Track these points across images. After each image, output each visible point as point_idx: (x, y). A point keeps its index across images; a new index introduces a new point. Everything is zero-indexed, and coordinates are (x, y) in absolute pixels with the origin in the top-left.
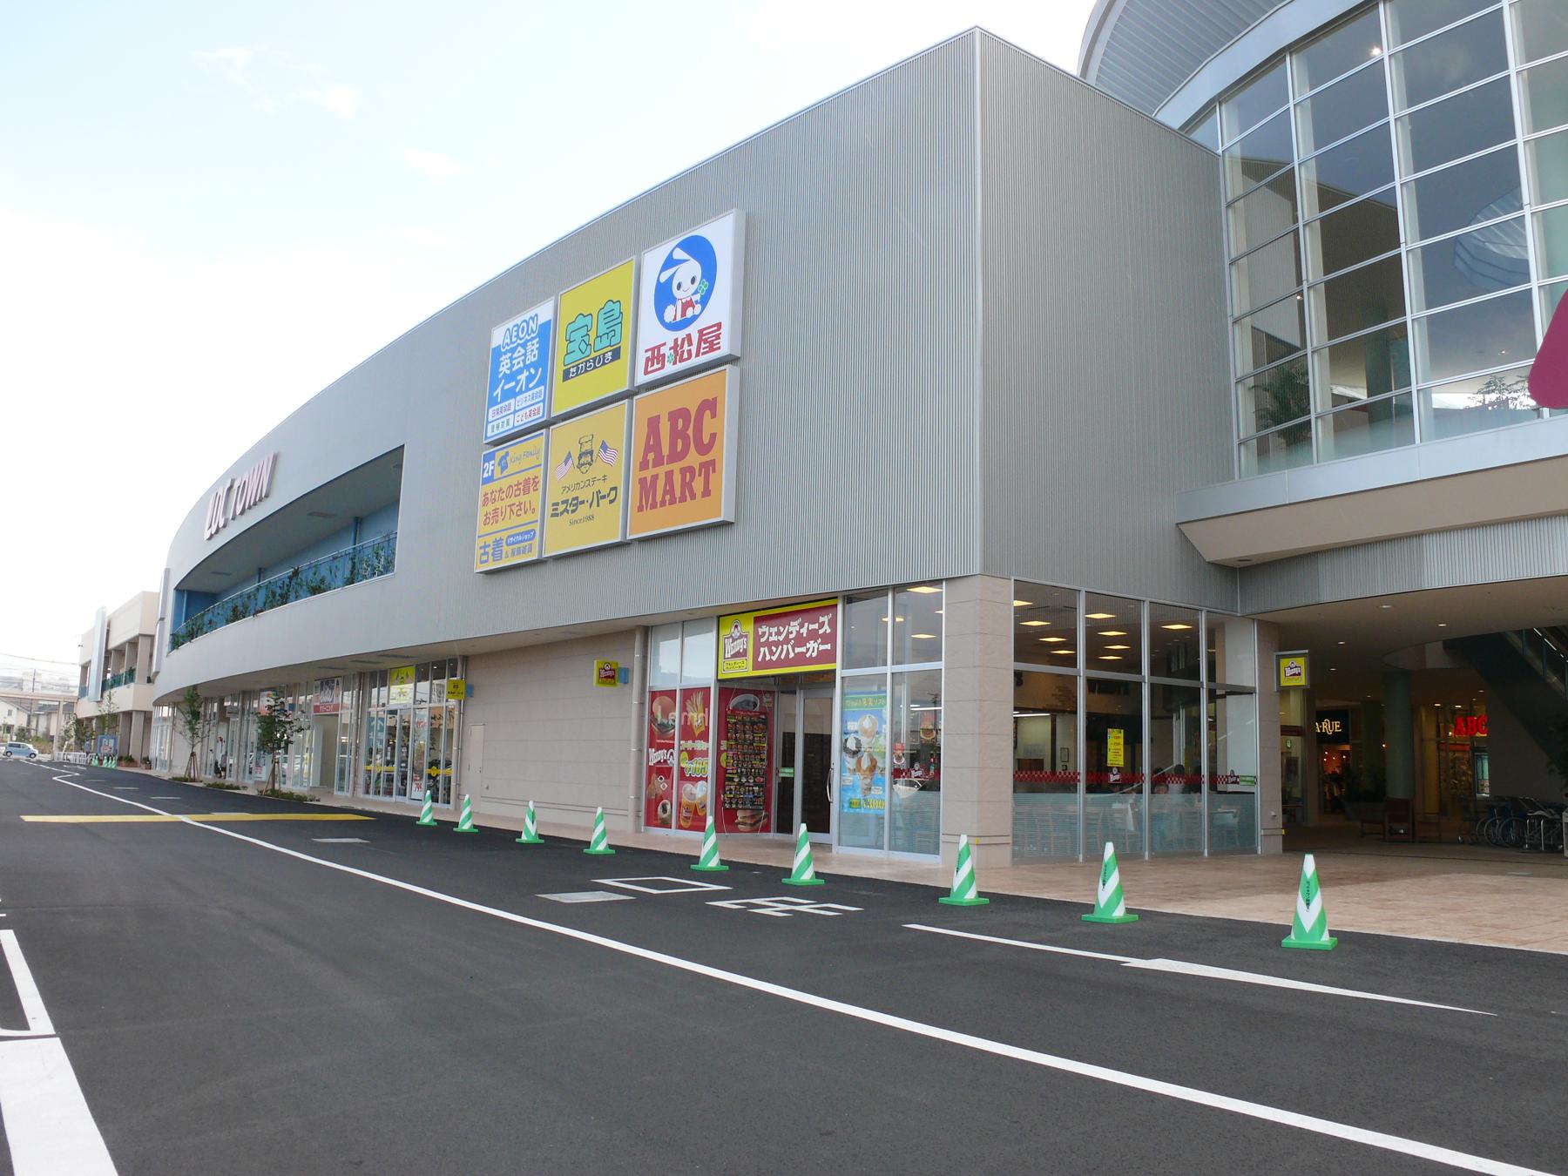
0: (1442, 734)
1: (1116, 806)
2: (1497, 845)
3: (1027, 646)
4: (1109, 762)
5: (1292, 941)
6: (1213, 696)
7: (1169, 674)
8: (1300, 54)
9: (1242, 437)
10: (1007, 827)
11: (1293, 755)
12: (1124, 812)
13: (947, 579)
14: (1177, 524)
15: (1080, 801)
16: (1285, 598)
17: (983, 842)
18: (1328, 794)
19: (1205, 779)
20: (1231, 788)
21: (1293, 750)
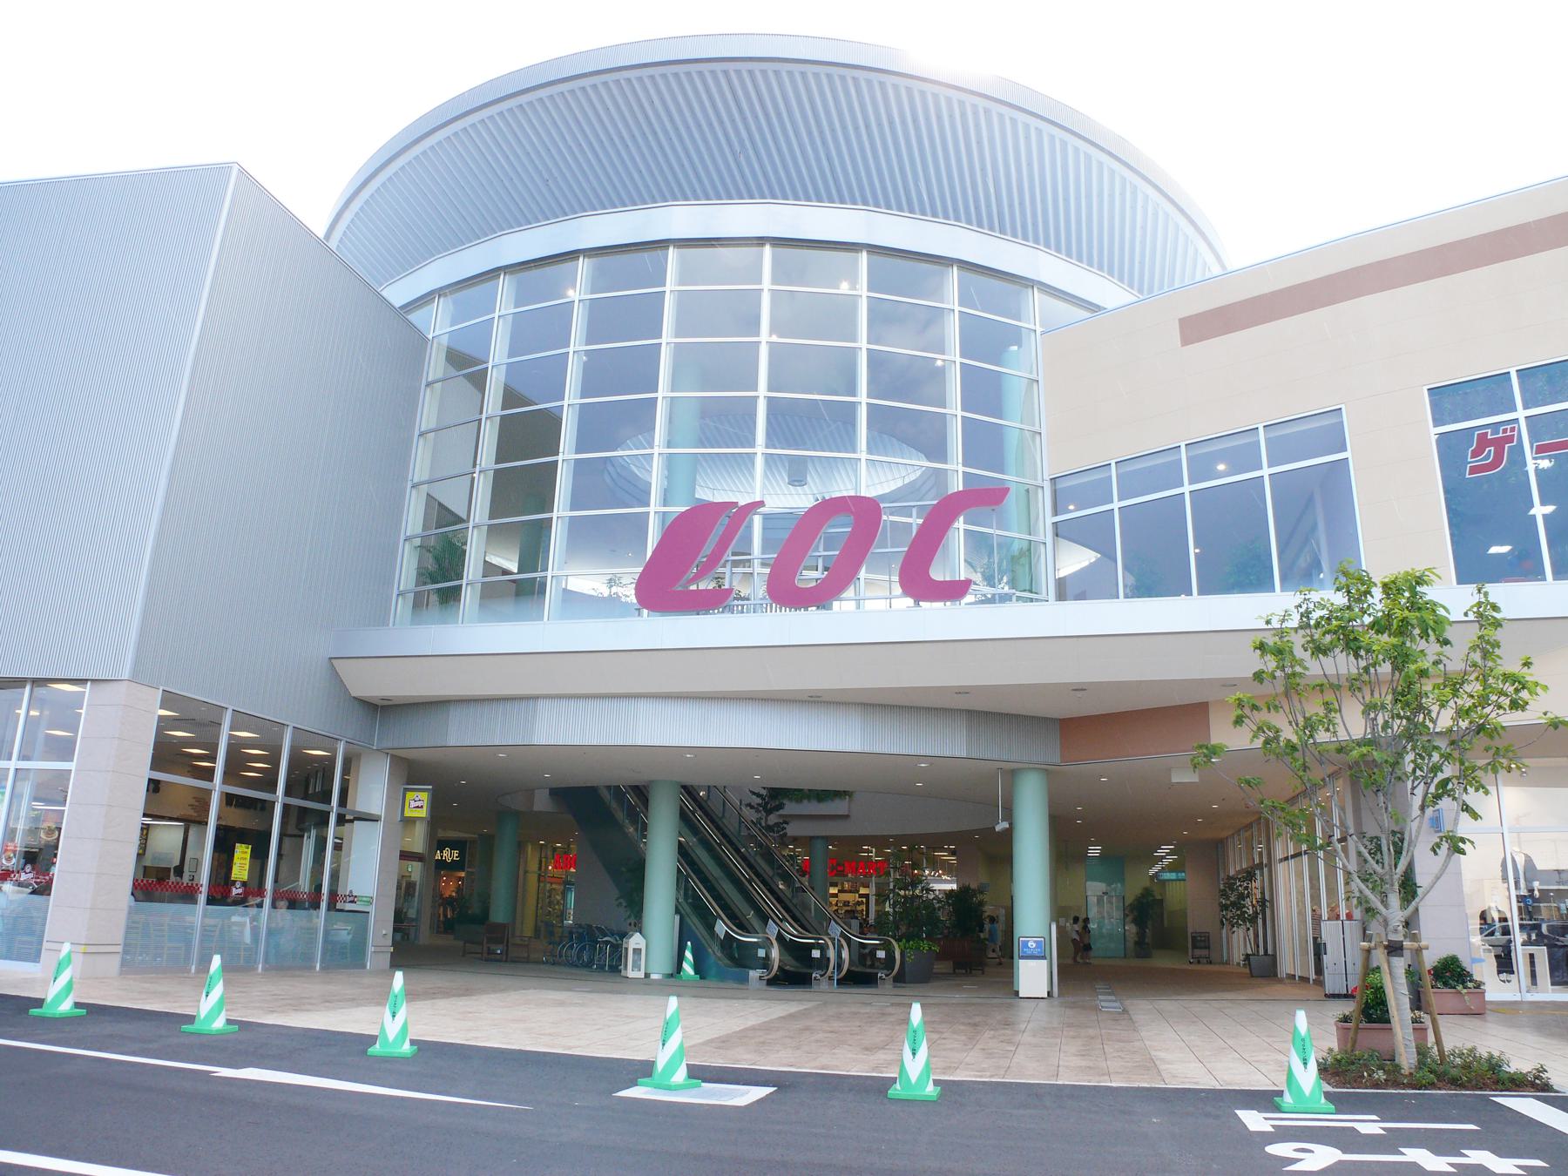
0: (543, 868)
1: (235, 919)
2: (574, 965)
3: (166, 755)
4: (233, 875)
5: (376, 1050)
6: (341, 820)
7: (306, 797)
8: (513, 276)
9: (401, 588)
10: (119, 937)
11: (412, 879)
12: (243, 925)
13: (92, 680)
14: (330, 658)
15: (199, 913)
16: (420, 739)
17: (92, 950)
18: (441, 916)
19: (325, 897)
20: (349, 907)
21: (413, 875)
